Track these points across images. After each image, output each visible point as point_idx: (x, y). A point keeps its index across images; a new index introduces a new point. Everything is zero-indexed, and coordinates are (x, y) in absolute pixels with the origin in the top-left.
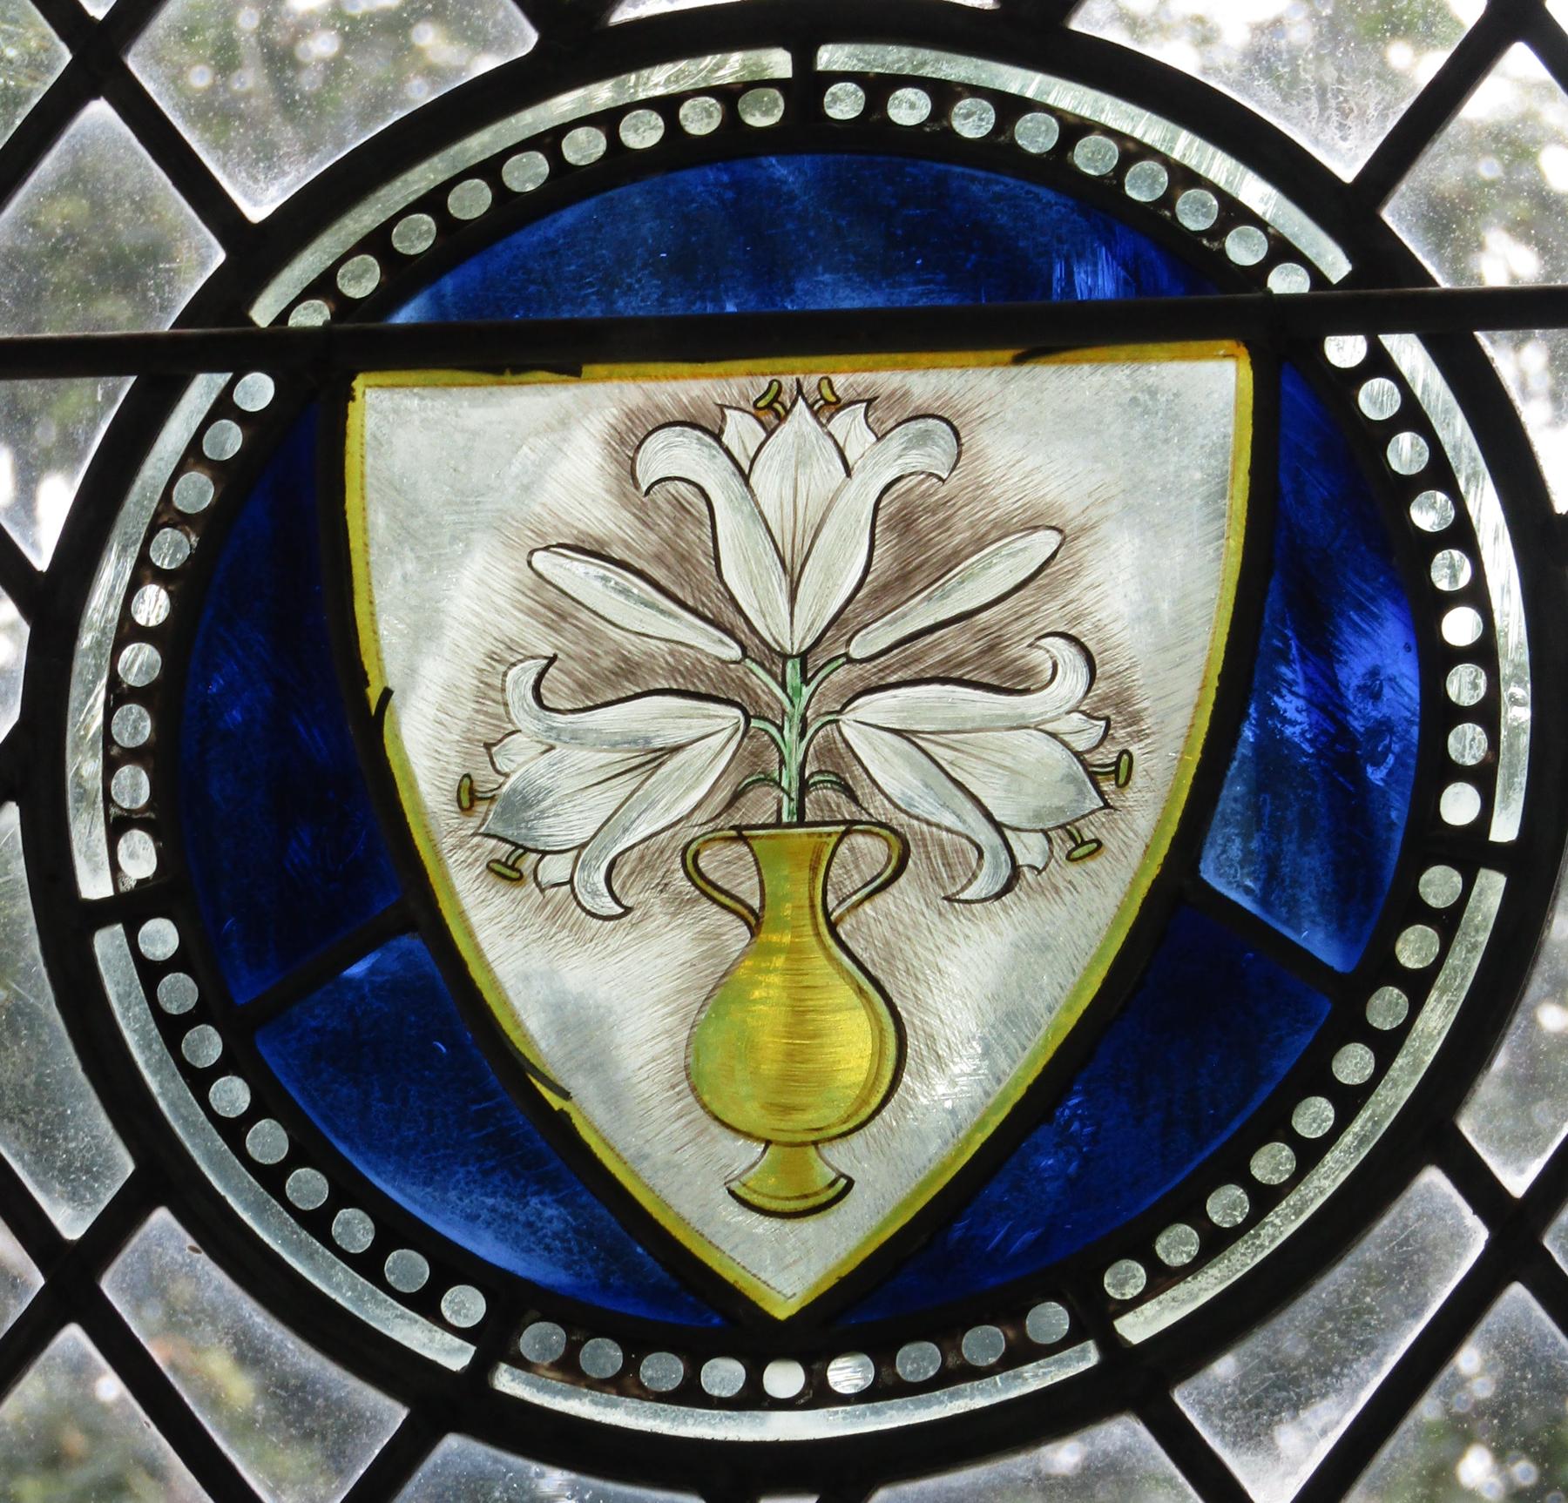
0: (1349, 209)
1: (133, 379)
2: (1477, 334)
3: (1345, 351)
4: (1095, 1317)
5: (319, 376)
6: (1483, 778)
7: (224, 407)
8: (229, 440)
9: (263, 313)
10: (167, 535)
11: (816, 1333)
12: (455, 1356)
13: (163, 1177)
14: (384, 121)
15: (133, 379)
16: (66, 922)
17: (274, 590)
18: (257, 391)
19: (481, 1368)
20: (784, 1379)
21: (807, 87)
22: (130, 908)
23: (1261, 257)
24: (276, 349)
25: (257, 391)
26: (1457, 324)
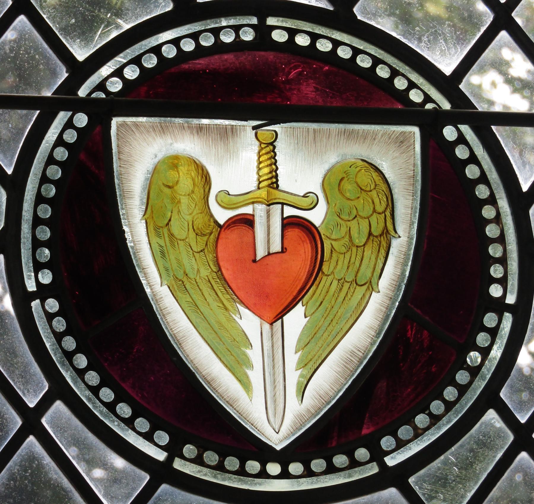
0: (449, 84)
1: (38, 112)
2: (493, 127)
3: (449, 133)
4: (378, 455)
5: (102, 110)
6: (503, 282)
7: (69, 125)
8: (71, 137)
9: (82, 92)
10: (54, 323)
11: (284, 457)
12: (161, 456)
13: (59, 390)
14: (140, 487)
15: (38, 112)
16: (21, 298)
17: (87, 189)
18: (82, 120)
19: (170, 460)
20: (274, 468)
21: (263, 31)
22: (43, 292)
23: (459, 382)
24: (86, 105)
25: (82, 120)
26: (485, 123)
